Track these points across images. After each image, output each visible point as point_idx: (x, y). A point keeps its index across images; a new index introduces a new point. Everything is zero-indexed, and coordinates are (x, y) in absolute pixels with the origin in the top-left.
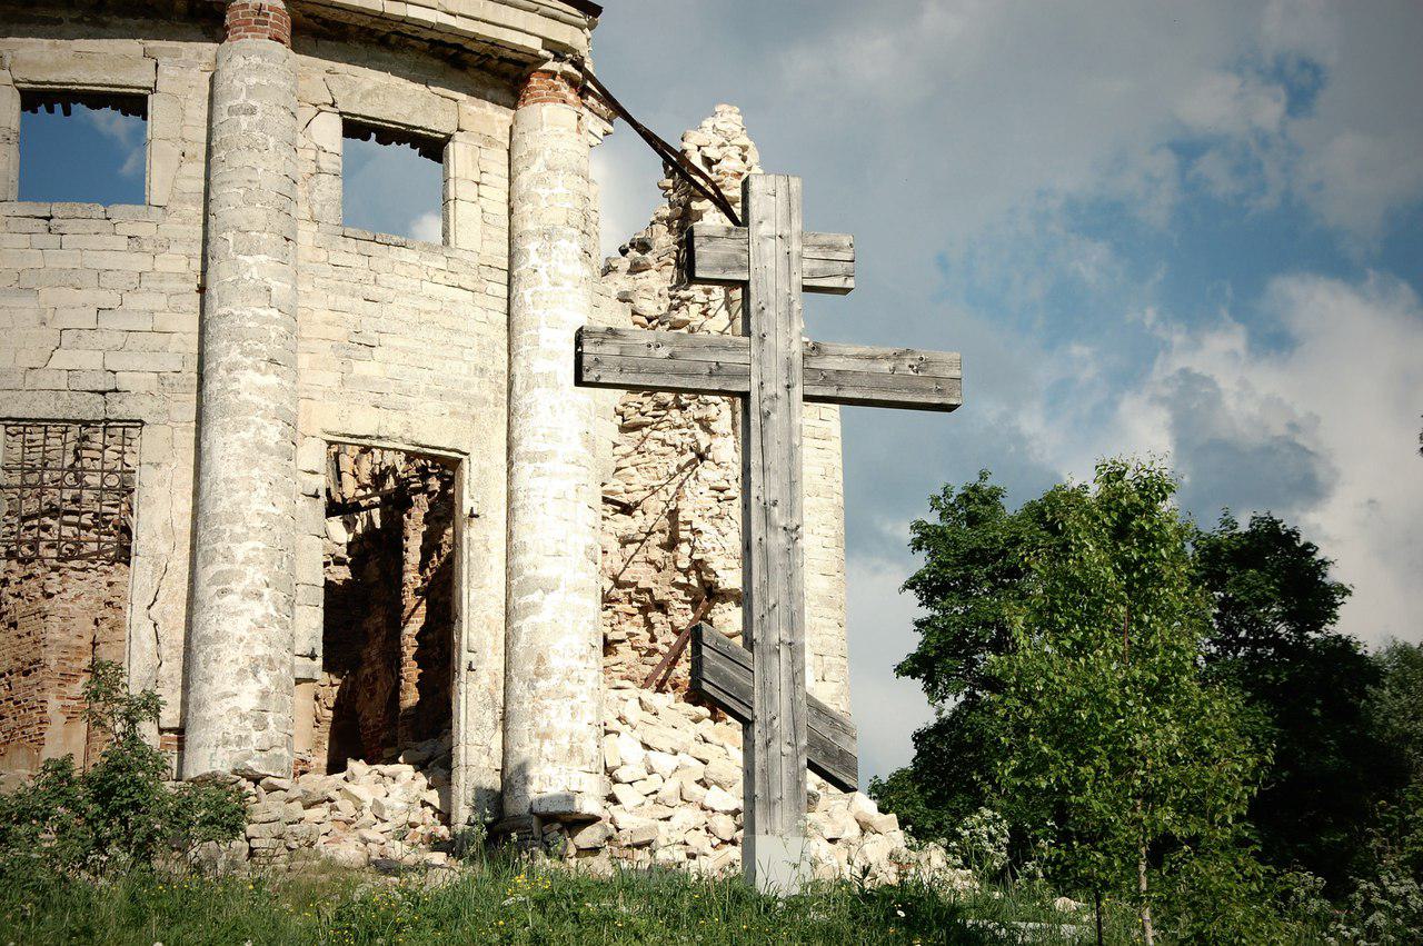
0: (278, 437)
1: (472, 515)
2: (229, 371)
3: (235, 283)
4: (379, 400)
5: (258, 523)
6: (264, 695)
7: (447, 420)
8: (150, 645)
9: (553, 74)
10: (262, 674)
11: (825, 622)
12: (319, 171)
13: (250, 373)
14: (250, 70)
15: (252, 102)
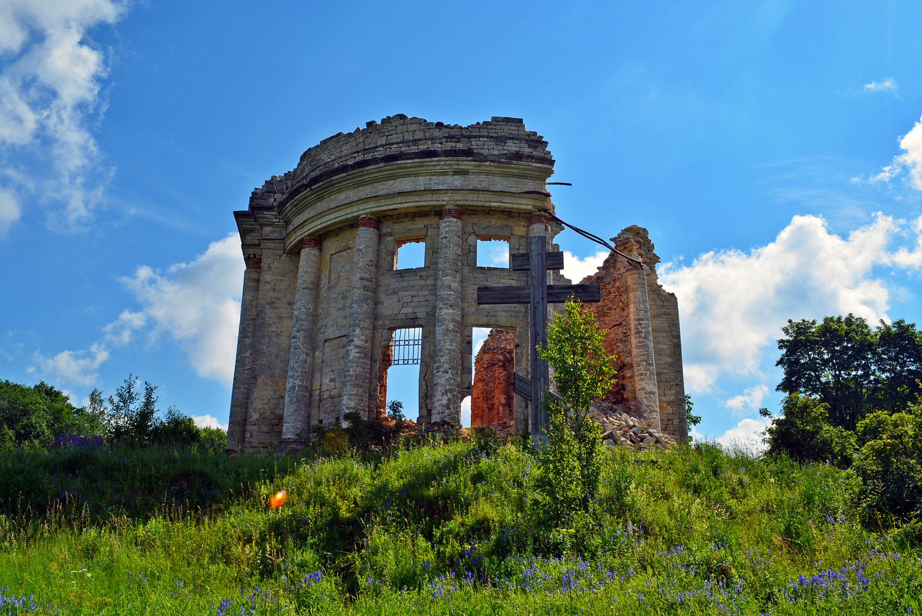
6: (449, 400)
14: (446, 227)
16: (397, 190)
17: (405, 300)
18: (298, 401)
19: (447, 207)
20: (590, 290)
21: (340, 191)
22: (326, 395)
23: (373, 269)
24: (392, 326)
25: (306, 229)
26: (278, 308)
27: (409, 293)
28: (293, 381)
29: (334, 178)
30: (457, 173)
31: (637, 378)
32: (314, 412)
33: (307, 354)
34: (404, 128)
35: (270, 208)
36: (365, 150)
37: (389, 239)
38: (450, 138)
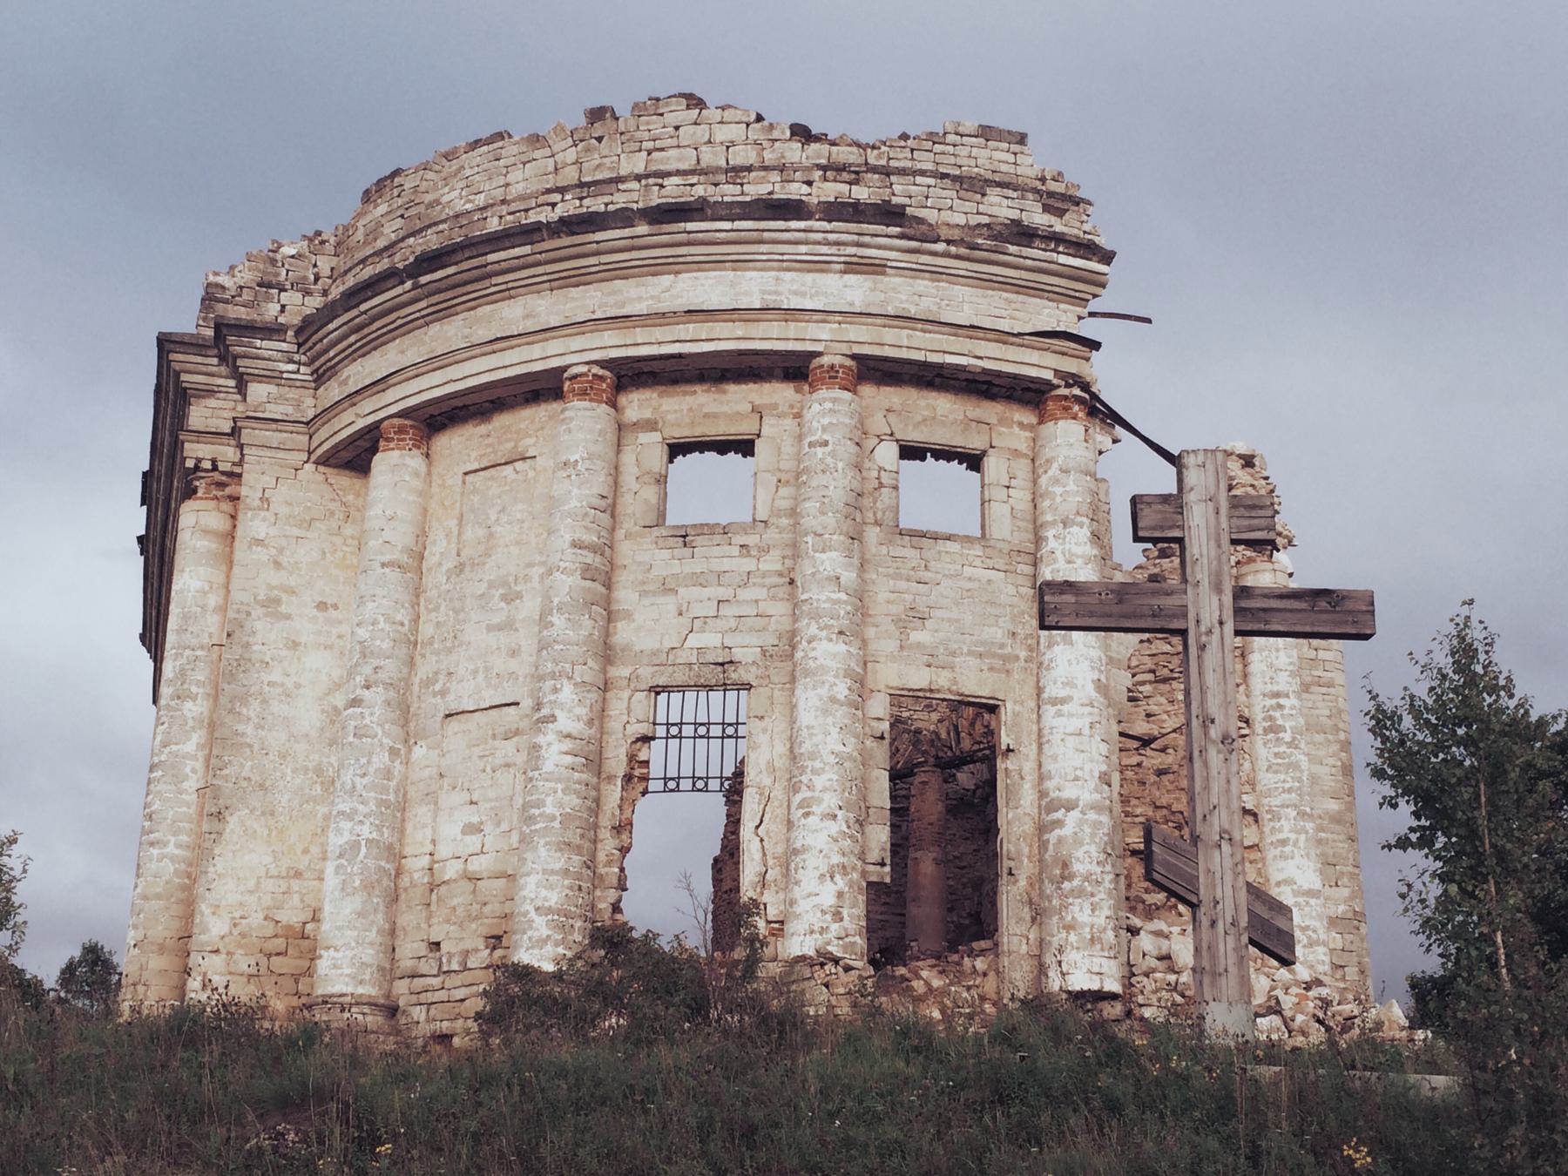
0: (847, 692)
1: (1009, 750)
2: (809, 642)
3: (813, 574)
4: (931, 660)
5: (832, 759)
6: (840, 895)
7: (986, 674)
8: (758, 856)
9: (1066, 398)
10: (838, 878)
11: (1336, 837)
12: (881, 485)
13: (824, 642)
14: (823, 414)
15: (826, 437)
16: (682, 303)
17: (698, 610)
18: (368, 887)
19: (826, 360)
20: (1350, 605)
21: (508, 294)
22: (451, 870)
23: (605, 518)
24: (662, 681)
25: (391, 395)
26: (288, 617)
27: (707, 592)
28: (355, 828)
29: (492, 257)
30: (854, 267)
31: (1271, 853)
32: (409, 918)
33: (393, 752)
34: (702, 132)
35: (273, 331)
36: (581, 185)
37: (645, 438)
38: (833, 169)
